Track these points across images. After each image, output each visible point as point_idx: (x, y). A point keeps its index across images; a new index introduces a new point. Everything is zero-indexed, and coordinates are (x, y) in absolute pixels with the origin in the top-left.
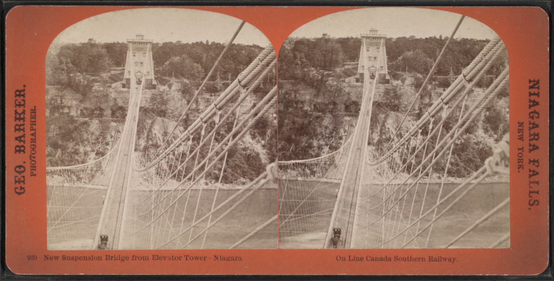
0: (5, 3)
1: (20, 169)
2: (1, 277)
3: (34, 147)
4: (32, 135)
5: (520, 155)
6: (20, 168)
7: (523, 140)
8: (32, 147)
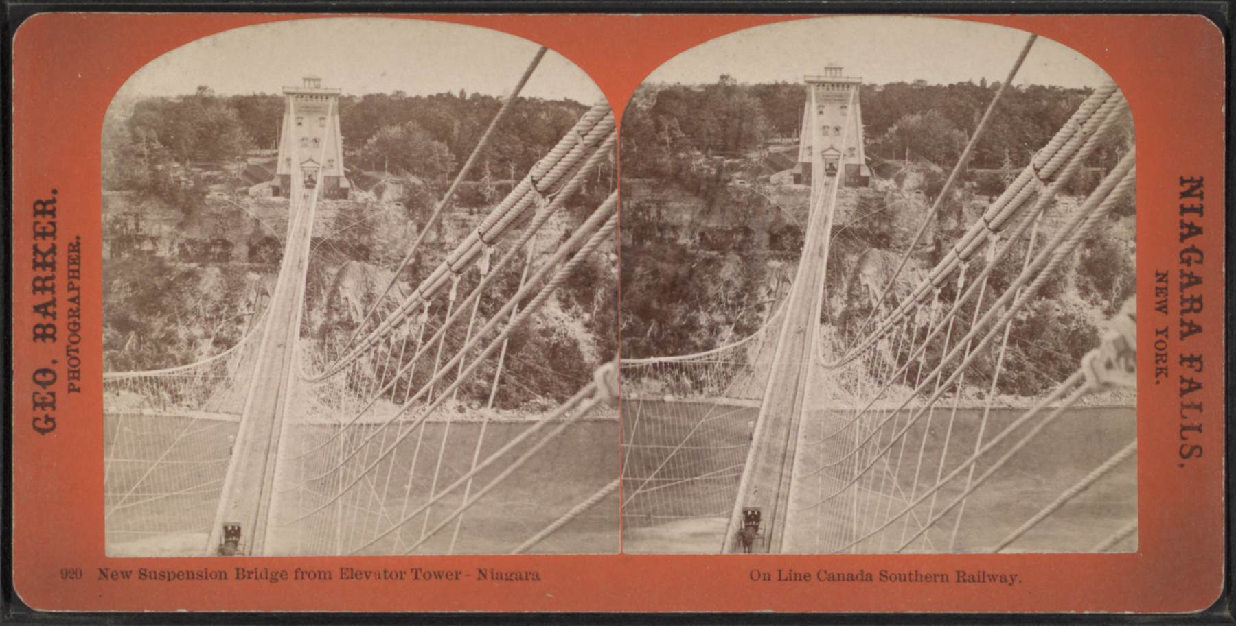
0: (11, 7)
1: (44, 375)
3: (77, 327)
4: (72, 300)
5: (1161, 345)
6: (44, 375)
7: (1166, 312)
8: (72, 327)
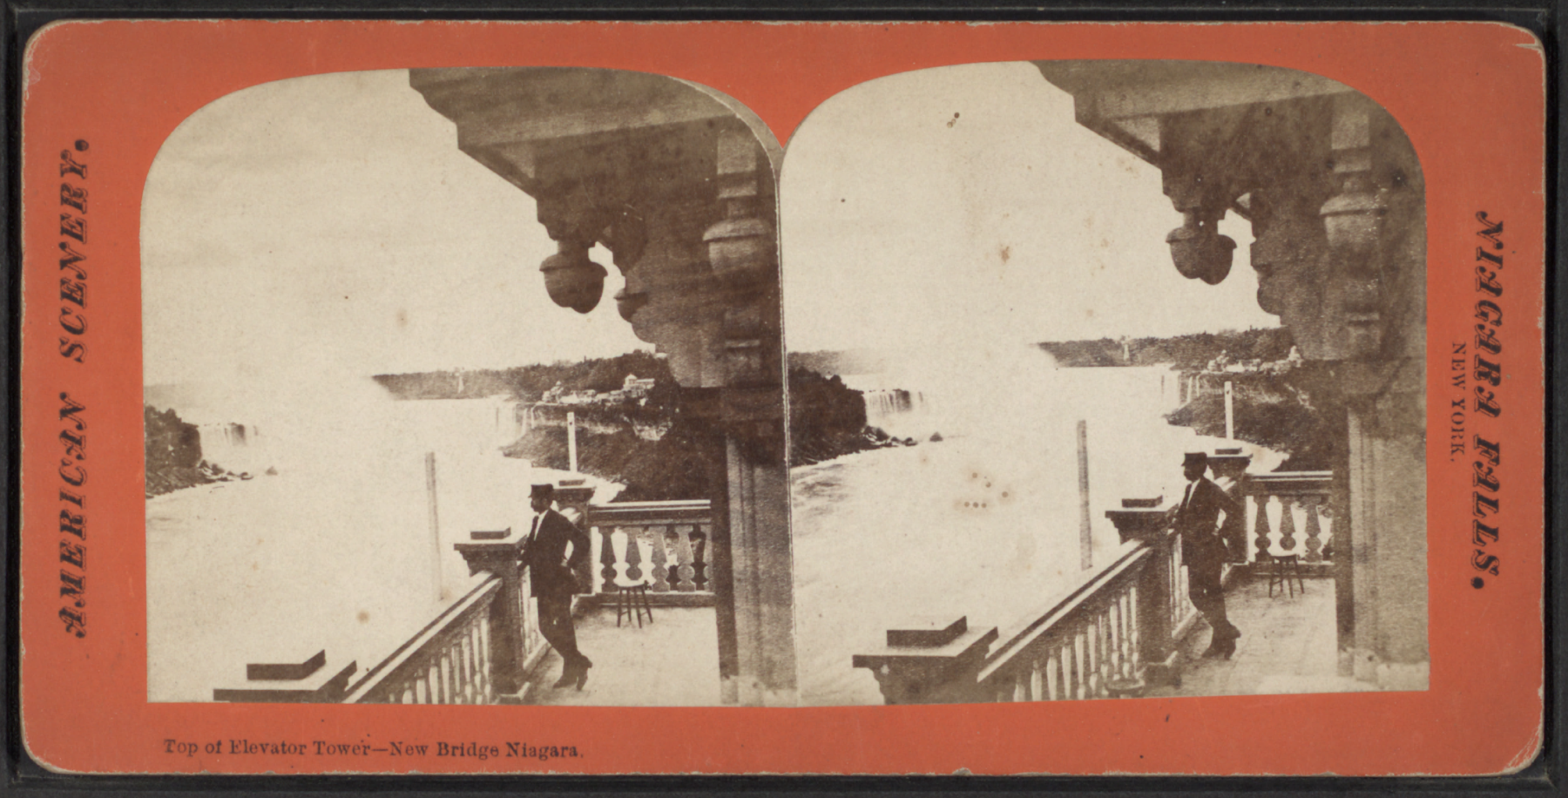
2: (10, 781)
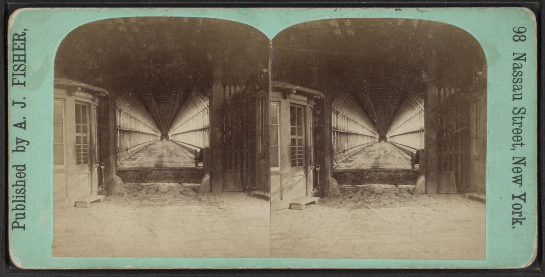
2: (6, 270)
